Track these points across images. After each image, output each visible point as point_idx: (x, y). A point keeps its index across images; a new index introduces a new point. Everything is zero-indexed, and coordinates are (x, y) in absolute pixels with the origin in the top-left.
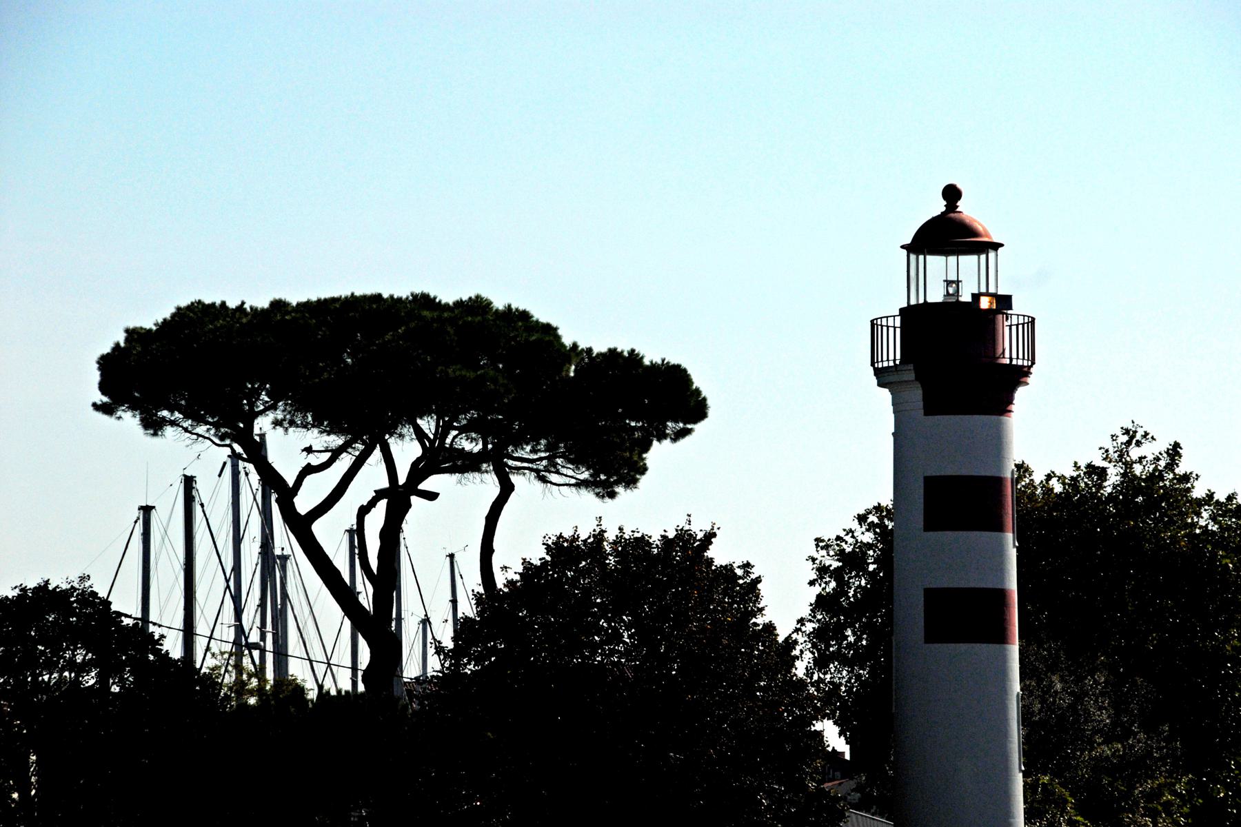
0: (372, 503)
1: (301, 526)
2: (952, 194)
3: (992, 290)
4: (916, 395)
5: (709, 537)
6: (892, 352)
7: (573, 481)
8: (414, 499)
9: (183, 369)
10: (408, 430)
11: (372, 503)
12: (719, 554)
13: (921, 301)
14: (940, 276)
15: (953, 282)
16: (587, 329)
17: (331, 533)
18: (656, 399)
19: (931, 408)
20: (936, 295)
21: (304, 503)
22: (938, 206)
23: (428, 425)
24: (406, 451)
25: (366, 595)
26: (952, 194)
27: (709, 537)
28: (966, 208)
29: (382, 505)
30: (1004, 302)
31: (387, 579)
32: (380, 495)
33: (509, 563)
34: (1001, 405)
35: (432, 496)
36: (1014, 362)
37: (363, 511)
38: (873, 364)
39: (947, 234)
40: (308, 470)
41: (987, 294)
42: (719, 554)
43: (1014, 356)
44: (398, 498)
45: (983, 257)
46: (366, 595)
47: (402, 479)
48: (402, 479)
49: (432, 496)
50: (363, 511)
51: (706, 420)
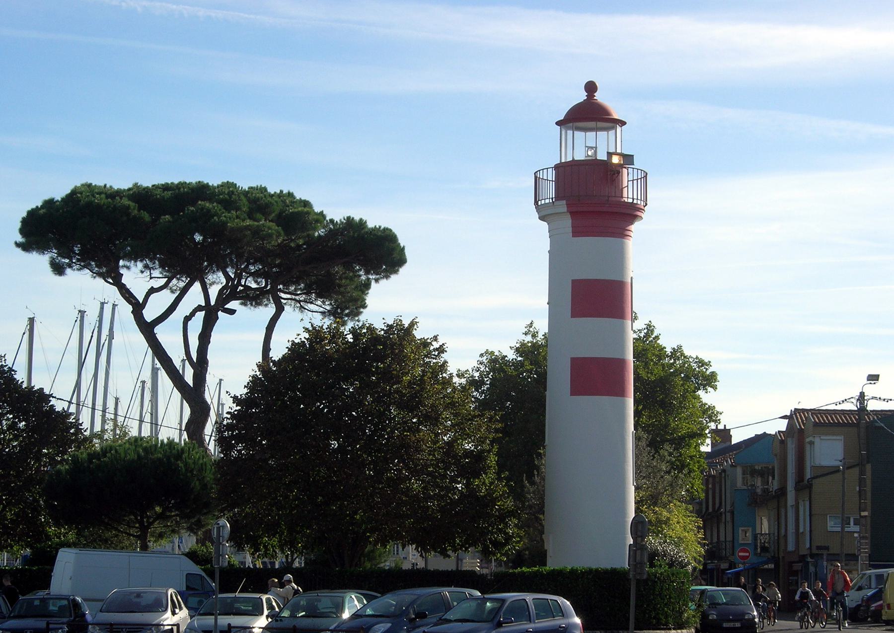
0: (193, 314)
1: (147, 329)
2: (591, 88)
3: (619, 151)
4: (567, 223)
5: (413, 324)
6: (549, 192)
7: (322, 310)
8: (220, 313)
9: (80, 230)
10: (220, 274)
11: (193, 314)
12: (419, 334)
13: (570, 159)
14: (584, 145)
15: (592, 148)
16: (334, 205)
17: (169, 336)
18: (379, 252)
19: (577, 232)
20: (580, 156)
21: (150, 314)
22: (582, 96)
23: (231, 272)
24: (217, 282)
25: (189, 376)
26: (591, 88)
27: (413, 324)
28: (599, 97)
29: (201, 315)
30: (628, 159)
31: (201, 365)
32: (199, 308)
33: (278, 351)
34: (621, 233)
35: (232, 312)
36: (635, 201)
37: (187, 319)
38: (536, 202)
39: (589, 114)
40: (152, 291)
41: (616, 154)
42: (419, 334)
43: (635, 197)
44: (211, 314)
45: (612, 132)
46: (189, 376)
47: (213, 303)
48: (213, 303)
49: (232, 312)
50: (187, 319)
51: (406, 264)
